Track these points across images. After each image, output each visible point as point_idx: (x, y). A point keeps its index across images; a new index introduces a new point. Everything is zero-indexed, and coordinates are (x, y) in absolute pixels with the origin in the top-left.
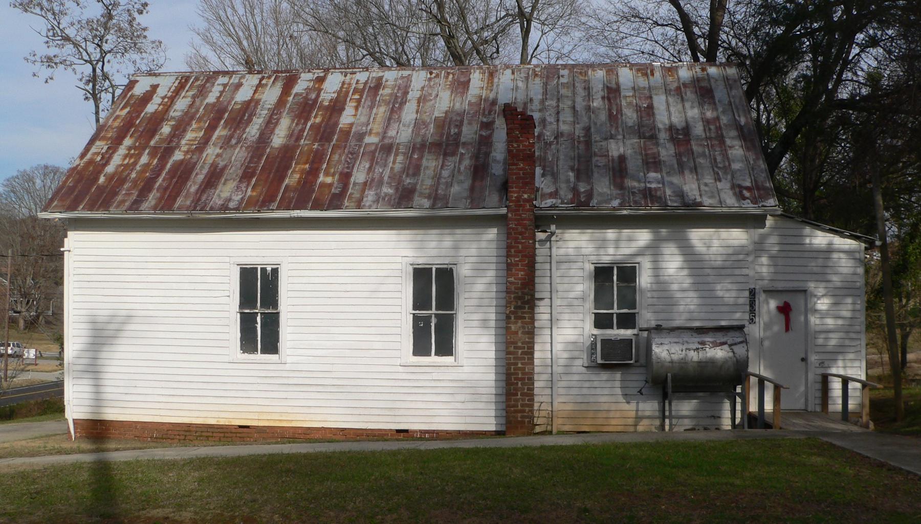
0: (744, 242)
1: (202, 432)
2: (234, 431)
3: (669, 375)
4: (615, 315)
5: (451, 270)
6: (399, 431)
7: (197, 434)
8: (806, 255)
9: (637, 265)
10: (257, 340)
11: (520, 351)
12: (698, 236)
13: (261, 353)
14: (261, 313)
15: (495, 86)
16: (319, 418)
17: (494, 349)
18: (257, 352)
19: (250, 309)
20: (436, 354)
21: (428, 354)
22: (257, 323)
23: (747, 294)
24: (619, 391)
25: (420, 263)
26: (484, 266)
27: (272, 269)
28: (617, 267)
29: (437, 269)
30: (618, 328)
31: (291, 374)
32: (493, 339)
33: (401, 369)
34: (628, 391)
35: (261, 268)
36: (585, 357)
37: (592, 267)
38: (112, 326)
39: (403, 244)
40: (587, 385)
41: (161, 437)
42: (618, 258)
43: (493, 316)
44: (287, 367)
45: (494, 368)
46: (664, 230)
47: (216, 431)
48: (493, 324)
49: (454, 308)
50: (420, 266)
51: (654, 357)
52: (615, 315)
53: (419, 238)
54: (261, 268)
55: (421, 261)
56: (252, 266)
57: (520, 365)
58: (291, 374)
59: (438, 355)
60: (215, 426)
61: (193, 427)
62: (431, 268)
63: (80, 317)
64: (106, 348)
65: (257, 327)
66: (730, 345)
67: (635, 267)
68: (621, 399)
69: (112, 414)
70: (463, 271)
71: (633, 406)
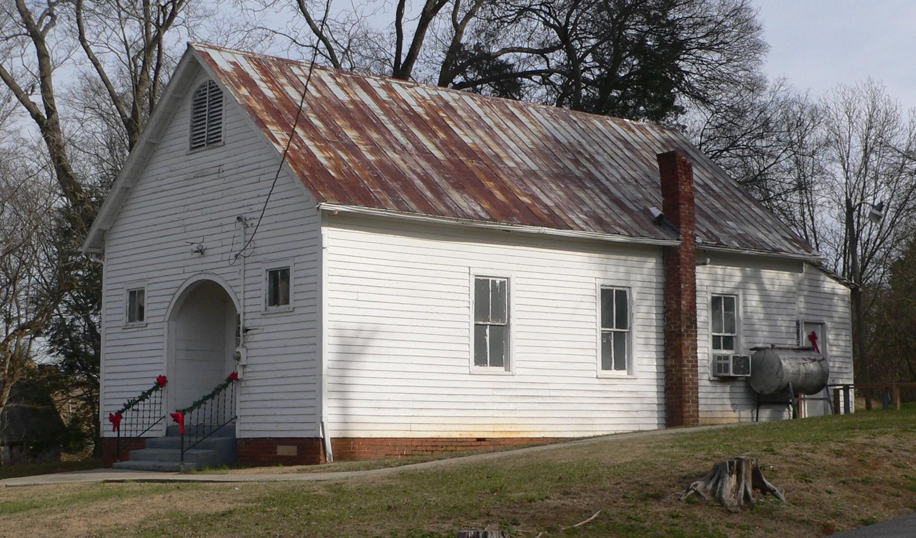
0: (791, 283)
1: (447, 446)
2: (474, 444)
3: (790, 384)
4: (722, 338)
5: (624, 292)
6: (479, 440)
7: (443, 449)
8: (818, 295)
9: (735, 297)
10: (487, 353)
11: (690, 364)
12: (768, 275)
13: (490, 366)
14: (490, 325)
15: (250, 505)
16: (540, 428)
17: (656, 364)
18: (487, 364)
19: (484, 321)
20: (615, 369)
21: (610, 369)
22: (486, 336)
23: (794, 324)
24: (728, 402)
25: (608, 284)
26: (647, 291)
27: (501, 282)
28: (724, 297)
29: (616, 291)
30: (724, 349)
31: (519, 386)
32: (654, 355)
33: (597, 381)
34: (737, 402)
35: (492, 281)
36: (709, 372)
37: (710, 298)
38: (359, 342)
39: (593, 267)
40: (711, 396)
41: (410, 453)
42: (725, 290)
43: (654, 335)
44: (516, 379)
45: (655, 381)
46: (748, 269)
47: (460, 444)
48: (653, 342)
49: (627, 327)
50: (606, 288)
51: (784, 369)
52: (722, 338)
53: (605, 261)
54: (492, 281)
55: (608, 283)
56: (485, 278)
57: (690, 377)
58: (519, 386)
59: (733, 346)
60: (458, 440)
61: (439, 441)
62: (613, 290)
63: (335, 323)
64: (353, 365)
65: (486, 340)
66: (819, 361)
67: (733, 298)
68: (729, 408)
69: (359, 432)
70: (634, 296)
71: (736, 415)
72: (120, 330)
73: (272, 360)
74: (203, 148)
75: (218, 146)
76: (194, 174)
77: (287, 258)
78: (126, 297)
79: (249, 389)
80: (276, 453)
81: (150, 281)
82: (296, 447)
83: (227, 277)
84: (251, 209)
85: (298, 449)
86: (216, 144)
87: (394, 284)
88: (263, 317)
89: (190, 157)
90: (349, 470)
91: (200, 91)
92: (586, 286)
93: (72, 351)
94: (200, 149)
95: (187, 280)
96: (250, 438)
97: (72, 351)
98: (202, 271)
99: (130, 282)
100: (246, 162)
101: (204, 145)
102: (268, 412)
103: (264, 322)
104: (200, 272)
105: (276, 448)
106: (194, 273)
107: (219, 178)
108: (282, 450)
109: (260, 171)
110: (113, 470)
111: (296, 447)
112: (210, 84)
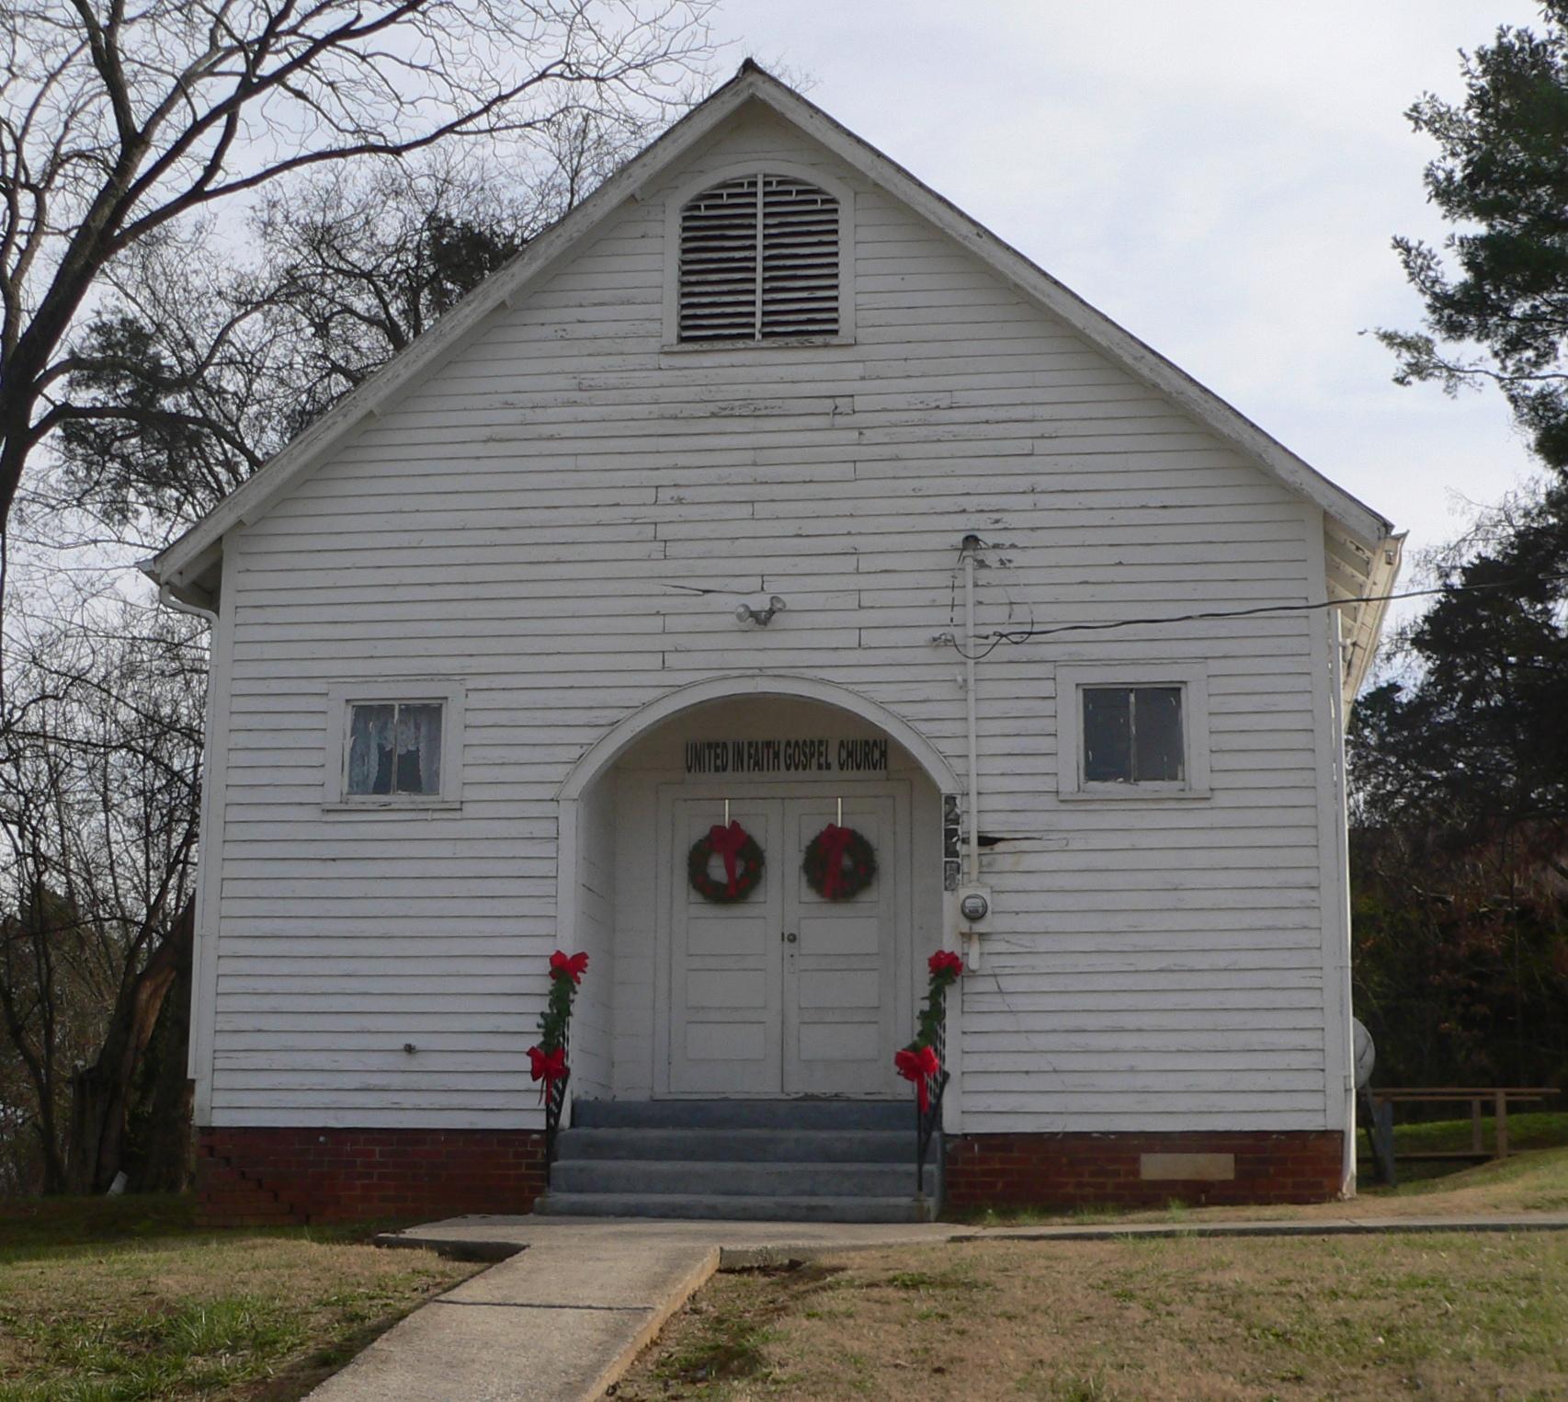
72: (312, 813)
73: (1119, 922)
74: (751, 343)
75: (826, 346)
76: (712, 407)
77: (1175, 661)
78: (346, 718)
79: (1008, 999)
80: (1136, 1173)
81: (471, 683)
82: (1232, 1156)
83: (885, 693)
84: (997, 521)
85: (1237, 1161)
86: (818, 340)
87: (437, 888)
88: (1063, 807)
89: (665, 361)
90: (1150, 1222)
91: (721, 196)
92: (524, 967)
93: (1460, 694)
94: (740, 344)
95: (681, 688)
96: (1058, 1133)
97: (1460, 694)
98: (760, 669)
99: (366, 679)
100: (961, 397)
101: (752, 336)
102: (1094, 1062)
103: (1068, 820)
104: (757, 672)
105: (1136, 1160)
106: (721, 673)
107: (832, 428)
108: (1154, 1167)
109: (1037, 429)
110: (540, 1218)
111: (1232, 1156)
112: (767, 184)
